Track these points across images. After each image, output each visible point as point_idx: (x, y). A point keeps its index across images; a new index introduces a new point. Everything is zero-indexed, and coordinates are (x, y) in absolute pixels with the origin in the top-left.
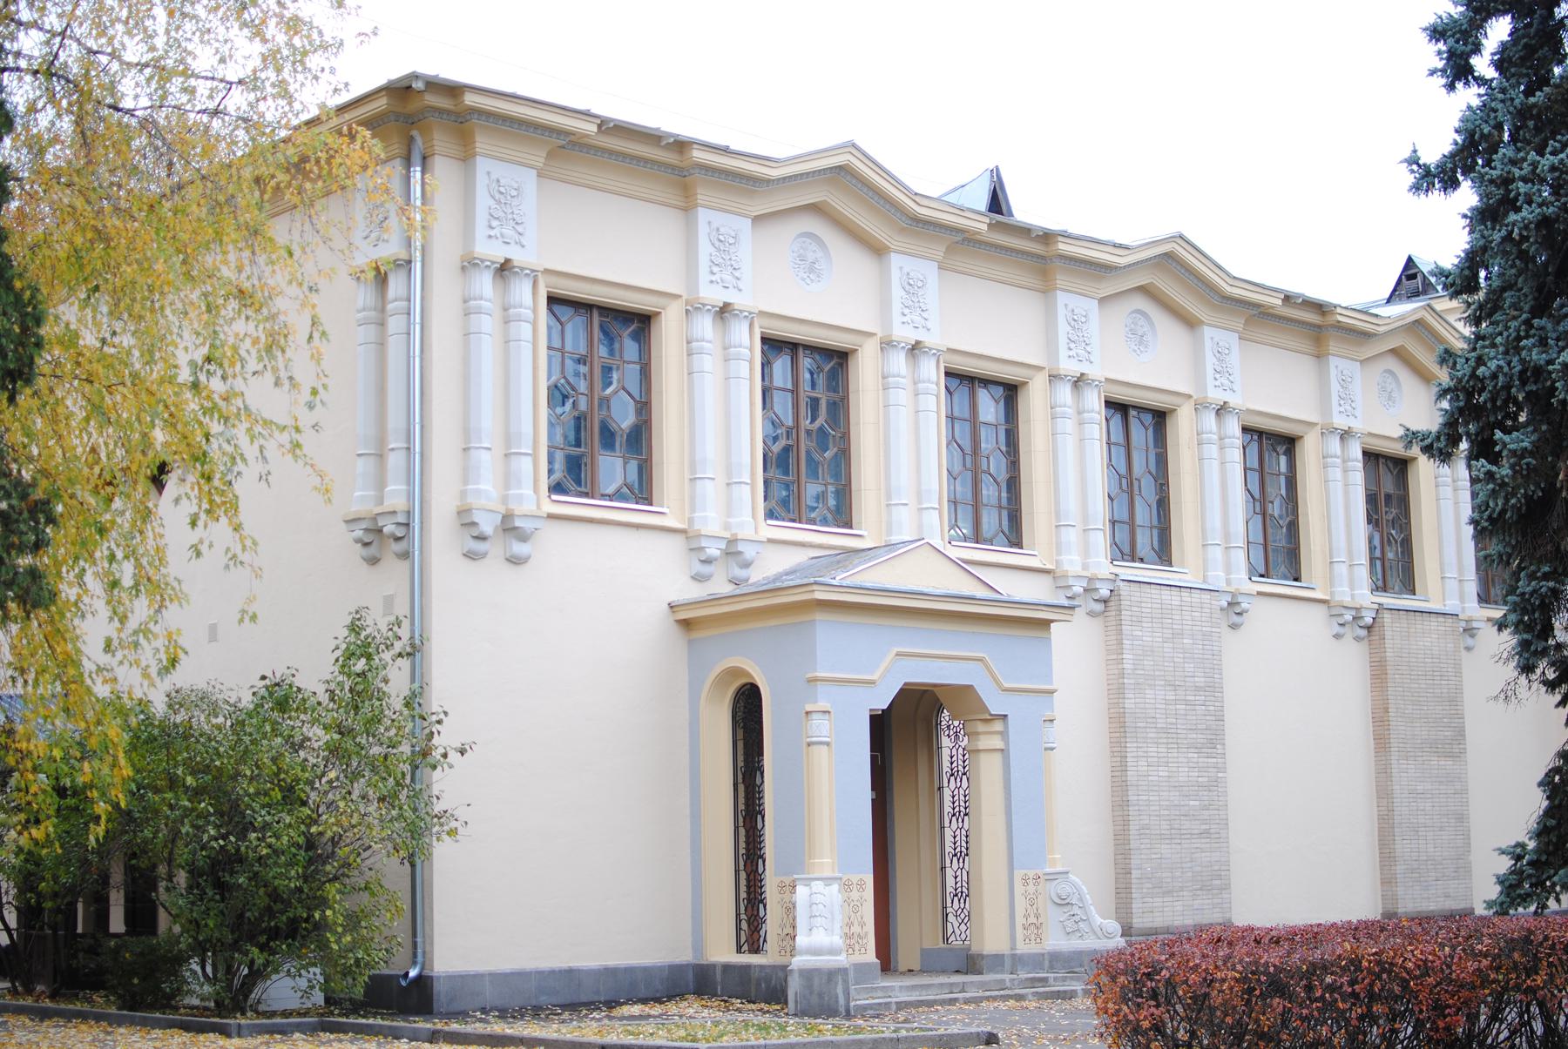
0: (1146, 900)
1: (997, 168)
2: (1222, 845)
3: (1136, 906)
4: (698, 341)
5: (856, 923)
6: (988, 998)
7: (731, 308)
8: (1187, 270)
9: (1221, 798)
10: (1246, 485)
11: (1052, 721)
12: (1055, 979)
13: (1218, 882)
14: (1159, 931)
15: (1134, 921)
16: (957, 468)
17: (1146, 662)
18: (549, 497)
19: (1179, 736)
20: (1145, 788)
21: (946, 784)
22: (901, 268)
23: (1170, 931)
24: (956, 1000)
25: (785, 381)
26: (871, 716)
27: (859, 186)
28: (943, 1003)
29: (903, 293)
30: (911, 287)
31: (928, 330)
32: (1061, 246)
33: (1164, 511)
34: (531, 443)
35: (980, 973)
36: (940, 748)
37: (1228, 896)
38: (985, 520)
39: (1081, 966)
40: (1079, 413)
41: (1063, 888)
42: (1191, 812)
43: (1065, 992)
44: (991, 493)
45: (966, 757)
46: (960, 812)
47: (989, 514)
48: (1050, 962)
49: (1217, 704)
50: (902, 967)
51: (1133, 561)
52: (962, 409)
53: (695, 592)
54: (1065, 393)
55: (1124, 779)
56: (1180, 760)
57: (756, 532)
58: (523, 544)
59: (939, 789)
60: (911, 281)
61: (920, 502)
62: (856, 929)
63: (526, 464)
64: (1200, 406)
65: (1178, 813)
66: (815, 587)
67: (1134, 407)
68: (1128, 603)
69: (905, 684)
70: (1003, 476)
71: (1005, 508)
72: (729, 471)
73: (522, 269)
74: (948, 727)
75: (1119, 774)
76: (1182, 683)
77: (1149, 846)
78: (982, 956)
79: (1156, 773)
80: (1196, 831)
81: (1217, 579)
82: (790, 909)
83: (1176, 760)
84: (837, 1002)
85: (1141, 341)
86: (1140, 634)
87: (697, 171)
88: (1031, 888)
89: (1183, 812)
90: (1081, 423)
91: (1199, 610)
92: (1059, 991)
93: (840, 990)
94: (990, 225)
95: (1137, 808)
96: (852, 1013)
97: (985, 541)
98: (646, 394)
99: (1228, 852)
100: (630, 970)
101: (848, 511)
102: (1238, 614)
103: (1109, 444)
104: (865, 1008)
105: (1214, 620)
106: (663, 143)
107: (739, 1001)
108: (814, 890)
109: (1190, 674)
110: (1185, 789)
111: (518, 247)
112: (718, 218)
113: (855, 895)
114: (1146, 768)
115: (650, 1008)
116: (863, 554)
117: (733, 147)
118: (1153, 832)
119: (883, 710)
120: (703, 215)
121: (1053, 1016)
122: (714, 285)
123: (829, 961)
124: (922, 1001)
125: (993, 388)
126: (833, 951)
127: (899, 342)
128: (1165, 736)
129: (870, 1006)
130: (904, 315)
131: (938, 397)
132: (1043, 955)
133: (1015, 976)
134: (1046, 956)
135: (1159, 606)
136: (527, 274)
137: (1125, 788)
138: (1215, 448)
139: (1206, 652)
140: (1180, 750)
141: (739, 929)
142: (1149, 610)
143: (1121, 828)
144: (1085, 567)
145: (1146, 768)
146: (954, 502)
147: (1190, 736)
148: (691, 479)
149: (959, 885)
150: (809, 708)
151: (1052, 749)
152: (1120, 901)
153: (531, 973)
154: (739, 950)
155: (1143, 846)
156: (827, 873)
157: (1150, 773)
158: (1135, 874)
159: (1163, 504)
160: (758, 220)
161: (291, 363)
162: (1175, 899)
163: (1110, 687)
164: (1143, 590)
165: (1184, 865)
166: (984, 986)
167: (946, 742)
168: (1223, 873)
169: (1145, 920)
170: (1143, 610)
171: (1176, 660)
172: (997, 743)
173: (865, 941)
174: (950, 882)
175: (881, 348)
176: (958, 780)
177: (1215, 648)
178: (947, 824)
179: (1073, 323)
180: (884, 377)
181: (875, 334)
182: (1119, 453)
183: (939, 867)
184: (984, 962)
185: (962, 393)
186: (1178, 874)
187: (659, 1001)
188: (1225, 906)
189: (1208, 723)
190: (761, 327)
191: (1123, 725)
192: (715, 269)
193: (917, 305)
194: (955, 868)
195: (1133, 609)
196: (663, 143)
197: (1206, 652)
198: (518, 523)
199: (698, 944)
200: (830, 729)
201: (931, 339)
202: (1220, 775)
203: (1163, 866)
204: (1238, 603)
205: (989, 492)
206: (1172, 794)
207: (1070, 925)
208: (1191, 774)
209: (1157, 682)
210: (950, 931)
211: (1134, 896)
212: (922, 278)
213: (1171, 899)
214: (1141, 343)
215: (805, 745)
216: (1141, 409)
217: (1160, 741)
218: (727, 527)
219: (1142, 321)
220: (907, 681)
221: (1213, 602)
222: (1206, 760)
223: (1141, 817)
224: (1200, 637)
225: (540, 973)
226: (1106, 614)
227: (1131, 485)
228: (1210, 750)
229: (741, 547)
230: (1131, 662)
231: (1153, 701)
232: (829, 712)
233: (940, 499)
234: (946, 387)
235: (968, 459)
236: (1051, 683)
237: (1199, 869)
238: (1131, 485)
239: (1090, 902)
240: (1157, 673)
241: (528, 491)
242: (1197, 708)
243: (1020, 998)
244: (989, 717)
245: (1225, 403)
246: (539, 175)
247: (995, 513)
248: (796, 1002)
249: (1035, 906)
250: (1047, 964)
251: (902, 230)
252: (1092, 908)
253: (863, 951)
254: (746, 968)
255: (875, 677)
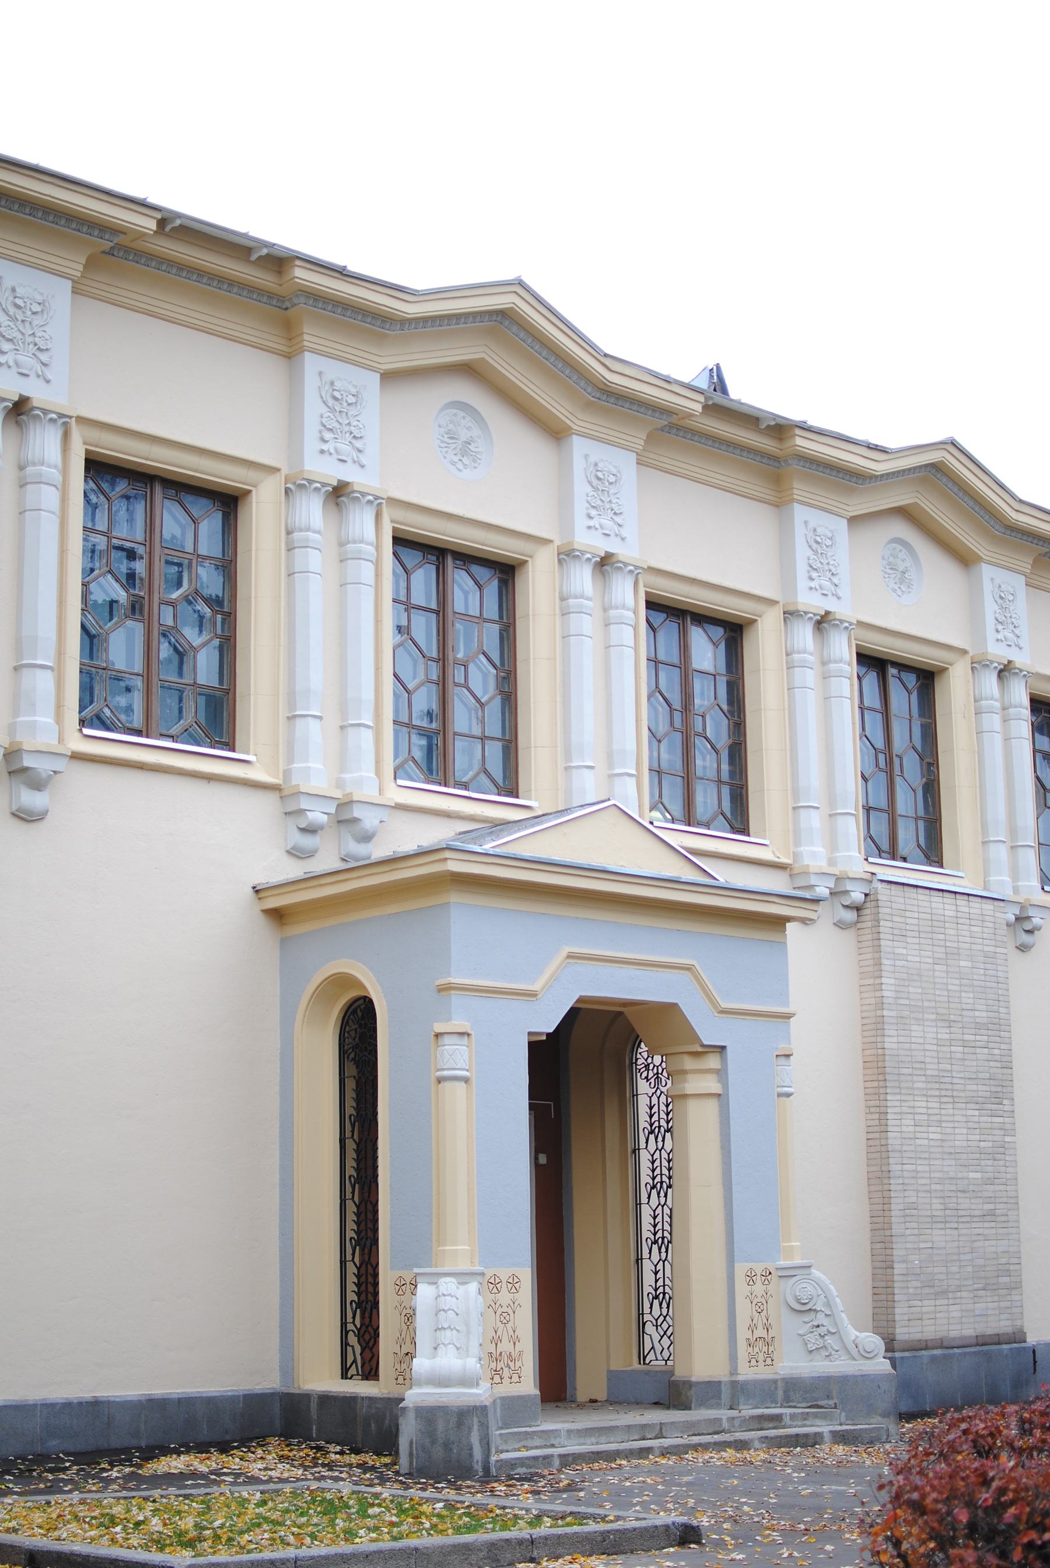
0: (912, 1303)
1: (718, 366)
2: (1011, 1230)
3: (900, 1312)
4: (301, 530)
5: (505, 1339)
6: (695, 1447)
7: (349, 490)
8: (960, 488)
9: (1009, 1170)
10: (1035, 772)
11: (788, 1056)
12: (793, 1417)
13: (1006, 1280)
14: (930, 1344)
15: (898, 1331)
16: (662, 728)
17: (911, 989)
18: (80, 730)
19: (955, 1087)
20: (912, 1155)
21: (643, 1145)
22: (586, 456)
23: (945, 1344)
24: (648, 1450)
25: (428, 599)
26: (530, 1044)
27: (530, 341)
28: (629, 1454)
29: (589, 489)
30: (599, 481)
31: (623, 539)
32: (799, 441)
33: (933, 798)
34: (52, 652)
35: (688, 1408)
36: (635, 1095)
37: (1018, 1298)
38: (699, 798)
39: (828, 1397)
40: (824, 663)
41: (803, 1289)
42: (971, 1188)
43: (806, 1436)
44: (708, 764)
45: (670, 1108)
46: (662, 1182)
47: (705, 792)
48: (784, 1392)
49: (1003, 1046)
50: (582, 1396)
51: (894, 859)
52: (669, 650)
53: (294, 870)
54: (804, 635)
55: (883, 1142)
56: (956, 1118)
57: (381, 791)
58: (37, 793)
59: (634, 1151)
60: (600, 475)
61: (611, 765)
62: (505, 1346)
63: (44, 682)
64: (978, 665)
65: (953, 1188)
66: (447, 854)
67: (895, 664)
68: (888, 910)
69: (581, 1000)
70: (723, 741)
71: (725, 783)
72: (343, 709)
73: (46, 412)
74: (647, 1067)
75: (877, 1135)
76: (959, 1019)
77: (916, 1231)
78: (689, 1384)
79: (925, 1135)
80: (976, 1213)
81: (1001, 884)
82: (410, 1317)
83: (951, 1119)
84: (471, 1455)
85: (902, 577)
86: (904, 951)
87: (302, 300)
88: (759, 1288)
89: (960, 1188)
90: (826, 677)
91: (980, 923)
92: (797, 1435)
93: (475, 1439)
94: (706, 407)
95: (901, 1181)
96: (493, 1471)
97: (699, 824)
98: (230, 601)
99: (1019, 1240)
100: (186, 1403)
101: (513, 775)
102: (1028, 932)
103: (862, 709)
104: (513, 1464)
105: (999, 938)
106: (254, 257)
107: (338, 1449)
108: (443, 1289)
109: (970, 1007)
110: (964, 1156)
111: (41, 383)
112: (333, 369)
113: (504, 1297)
114: (912, 1129)
115: (202, 1461)
116: (524, 823)
117: (353, 267)
118: (921, 1213)
119: (548, 1035)
120: (311, 363)
121: (788, 1480)
122: (326, 456)
123: (458, 1395)
124: (598, 1453)
125: (711, 628)
126: (466, 1381)
127: (583, 553)
128: (937, 1086)
129: (521, 1462)
130: (590, 517)
131: (635, 629)
132: (775, 1382)
133: (734, 1413)
134: (780, 1384)
135: (928, 917)
136: (51, 420)
137: (884, 1155)
138: (997, 719)
139: (988, 978)
140: (957, 1105)
141: (344, 1344)
142: (915, 922)
143: (880, 1207)
144: (832, 862)
145: (912, 1129)
146: (658, 772)
147: (969, 1087)
148: (289, 718)
149: (660, 1283)
150: (439, 1028)
151: (789, 1095)
152: (879, 1304)
153: (35, 1405)
154: (345, 1375)
155: (908, 1232)
156: (464, 1266)
157: (918, 1135)
158: (899, 1268)
159: (931, 790)
160: (389, 377)
161: (466, 1037)
162: (951, 1302)
163: (865, 1021)
164: (907, 895)
165: (962, 1257)
166: (692, 1429)
167: (643, 1087)
168: (1012, 1267)
169: (912, 1330)
170: (909, 921)
171: (950, 987)
172: (711, 1084)
173: (518, 1364)
174: (648, 1279)
175: (559, 561)
176: (660, 1138)
177: (1000, 974)
178: (644, 1199)
179: (815, 546)
180: (563, 599)
181: (551, 541)
182: (874, 722)
183: (633, 1258)
184: (693, 1392)
185: (669, 631)
186: (955, 1269)
187: (224, 1448)
188: (1014, 1310)
189: (992, 1071)
190: (392, 521)
191: (882, 1071)
192: (328, 436)
193: (608, 506)
194: (655, 1261)
195: (895, 919)
196: (254, 257)
197: (988, 978)
198: (28, 762)
199: (288, 1367)
200: (470, 1058)
201: (627, 552)
202: (1007, 1139)
203: (935, 1258)
204: (1029, 918)
205: (705, 762)
206: (946, 1163)
207: (813, 1340)
208: (971, 1137)
209: (926, 1016)
210: (648, 1346)
211: (897, 1298)
212: (614, 471)
213: (946, 1302)
214: (902, 581)
215: (433, 1080)
216: (904, 667)
217: (930, 1093)
218: (340, 784)
219: (903, 554)
220: (583, 994)
221: (998, 915)
222: (989, 1119)
223: (907, 1194)
224: (982, 959)
225: (49, 1407)
226: (859, 925)
227: (890, 762)
228: (993, 1107)
229: (357, 812)
230: (893, 988)
231: (921, 1041)
232: (469, 1035)
233: (638, 764)
234: (648, 621)
235: (677, 716)
236: (786, 1004)
237: (981, 1262)
238: (890, 762)
239: (841, 1308)
240: (926, 1004)
241: (45, 719)
242: (978, 1050)
243: (741, 1445)
244: (700, 1049)
245: (1010, 662)
246: (75, 291)
247: (713, 789)
248: (411, 1455)
249: (764, 1314)
250: (780, 1393)
251: (588, 406)
252: (843, 1315)
253: (515, 1378)
254: (350, 1402)
255: (536, 987)
